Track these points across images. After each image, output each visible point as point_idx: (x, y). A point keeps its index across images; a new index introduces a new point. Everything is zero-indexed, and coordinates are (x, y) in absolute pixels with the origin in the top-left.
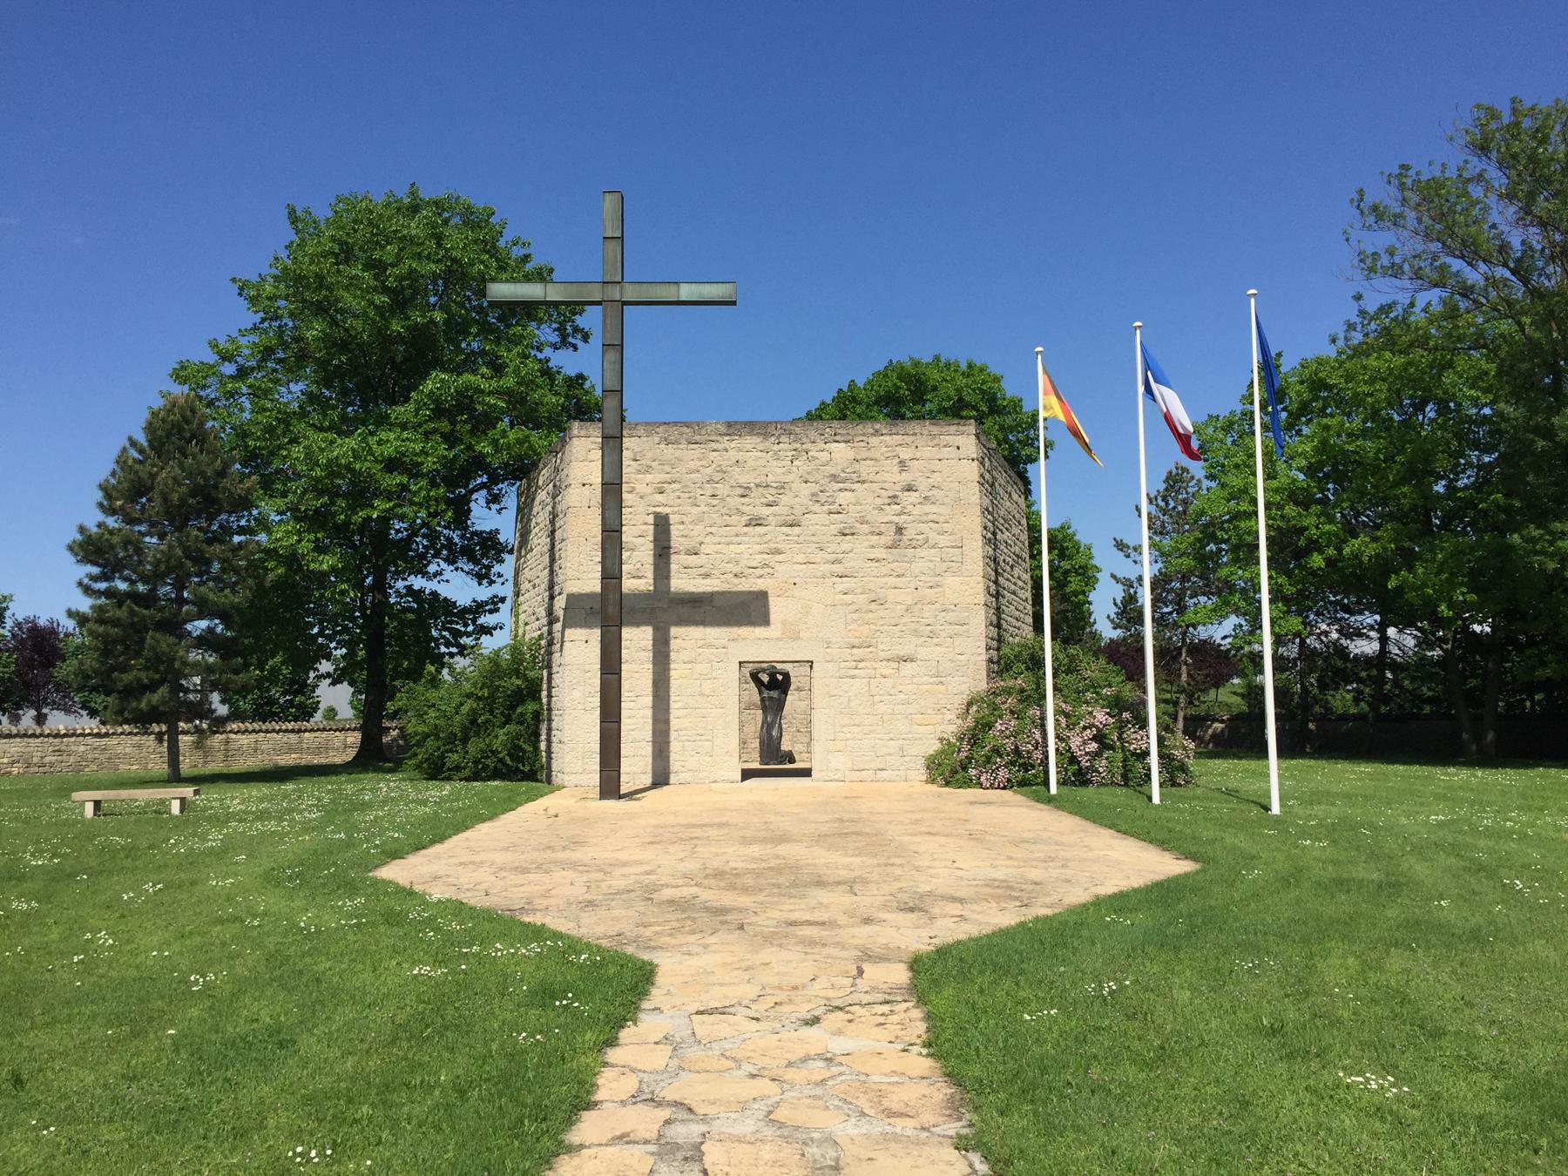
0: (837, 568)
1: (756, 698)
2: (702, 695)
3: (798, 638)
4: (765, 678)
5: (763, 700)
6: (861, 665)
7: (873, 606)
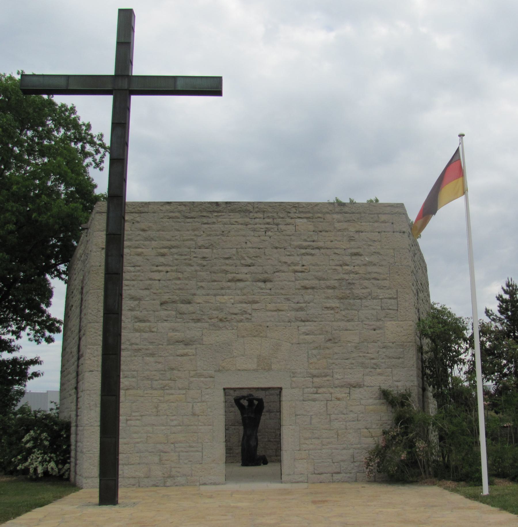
0: (301, 314)
1: (239, 417)
2: (194, 414)
3: (270, 369)
4: (245, 403)
5: (244, 419)
6: (320, 390)
7: (329, 344)
